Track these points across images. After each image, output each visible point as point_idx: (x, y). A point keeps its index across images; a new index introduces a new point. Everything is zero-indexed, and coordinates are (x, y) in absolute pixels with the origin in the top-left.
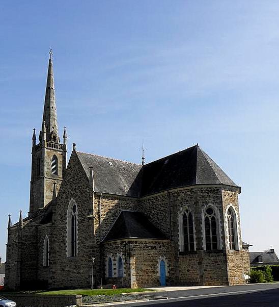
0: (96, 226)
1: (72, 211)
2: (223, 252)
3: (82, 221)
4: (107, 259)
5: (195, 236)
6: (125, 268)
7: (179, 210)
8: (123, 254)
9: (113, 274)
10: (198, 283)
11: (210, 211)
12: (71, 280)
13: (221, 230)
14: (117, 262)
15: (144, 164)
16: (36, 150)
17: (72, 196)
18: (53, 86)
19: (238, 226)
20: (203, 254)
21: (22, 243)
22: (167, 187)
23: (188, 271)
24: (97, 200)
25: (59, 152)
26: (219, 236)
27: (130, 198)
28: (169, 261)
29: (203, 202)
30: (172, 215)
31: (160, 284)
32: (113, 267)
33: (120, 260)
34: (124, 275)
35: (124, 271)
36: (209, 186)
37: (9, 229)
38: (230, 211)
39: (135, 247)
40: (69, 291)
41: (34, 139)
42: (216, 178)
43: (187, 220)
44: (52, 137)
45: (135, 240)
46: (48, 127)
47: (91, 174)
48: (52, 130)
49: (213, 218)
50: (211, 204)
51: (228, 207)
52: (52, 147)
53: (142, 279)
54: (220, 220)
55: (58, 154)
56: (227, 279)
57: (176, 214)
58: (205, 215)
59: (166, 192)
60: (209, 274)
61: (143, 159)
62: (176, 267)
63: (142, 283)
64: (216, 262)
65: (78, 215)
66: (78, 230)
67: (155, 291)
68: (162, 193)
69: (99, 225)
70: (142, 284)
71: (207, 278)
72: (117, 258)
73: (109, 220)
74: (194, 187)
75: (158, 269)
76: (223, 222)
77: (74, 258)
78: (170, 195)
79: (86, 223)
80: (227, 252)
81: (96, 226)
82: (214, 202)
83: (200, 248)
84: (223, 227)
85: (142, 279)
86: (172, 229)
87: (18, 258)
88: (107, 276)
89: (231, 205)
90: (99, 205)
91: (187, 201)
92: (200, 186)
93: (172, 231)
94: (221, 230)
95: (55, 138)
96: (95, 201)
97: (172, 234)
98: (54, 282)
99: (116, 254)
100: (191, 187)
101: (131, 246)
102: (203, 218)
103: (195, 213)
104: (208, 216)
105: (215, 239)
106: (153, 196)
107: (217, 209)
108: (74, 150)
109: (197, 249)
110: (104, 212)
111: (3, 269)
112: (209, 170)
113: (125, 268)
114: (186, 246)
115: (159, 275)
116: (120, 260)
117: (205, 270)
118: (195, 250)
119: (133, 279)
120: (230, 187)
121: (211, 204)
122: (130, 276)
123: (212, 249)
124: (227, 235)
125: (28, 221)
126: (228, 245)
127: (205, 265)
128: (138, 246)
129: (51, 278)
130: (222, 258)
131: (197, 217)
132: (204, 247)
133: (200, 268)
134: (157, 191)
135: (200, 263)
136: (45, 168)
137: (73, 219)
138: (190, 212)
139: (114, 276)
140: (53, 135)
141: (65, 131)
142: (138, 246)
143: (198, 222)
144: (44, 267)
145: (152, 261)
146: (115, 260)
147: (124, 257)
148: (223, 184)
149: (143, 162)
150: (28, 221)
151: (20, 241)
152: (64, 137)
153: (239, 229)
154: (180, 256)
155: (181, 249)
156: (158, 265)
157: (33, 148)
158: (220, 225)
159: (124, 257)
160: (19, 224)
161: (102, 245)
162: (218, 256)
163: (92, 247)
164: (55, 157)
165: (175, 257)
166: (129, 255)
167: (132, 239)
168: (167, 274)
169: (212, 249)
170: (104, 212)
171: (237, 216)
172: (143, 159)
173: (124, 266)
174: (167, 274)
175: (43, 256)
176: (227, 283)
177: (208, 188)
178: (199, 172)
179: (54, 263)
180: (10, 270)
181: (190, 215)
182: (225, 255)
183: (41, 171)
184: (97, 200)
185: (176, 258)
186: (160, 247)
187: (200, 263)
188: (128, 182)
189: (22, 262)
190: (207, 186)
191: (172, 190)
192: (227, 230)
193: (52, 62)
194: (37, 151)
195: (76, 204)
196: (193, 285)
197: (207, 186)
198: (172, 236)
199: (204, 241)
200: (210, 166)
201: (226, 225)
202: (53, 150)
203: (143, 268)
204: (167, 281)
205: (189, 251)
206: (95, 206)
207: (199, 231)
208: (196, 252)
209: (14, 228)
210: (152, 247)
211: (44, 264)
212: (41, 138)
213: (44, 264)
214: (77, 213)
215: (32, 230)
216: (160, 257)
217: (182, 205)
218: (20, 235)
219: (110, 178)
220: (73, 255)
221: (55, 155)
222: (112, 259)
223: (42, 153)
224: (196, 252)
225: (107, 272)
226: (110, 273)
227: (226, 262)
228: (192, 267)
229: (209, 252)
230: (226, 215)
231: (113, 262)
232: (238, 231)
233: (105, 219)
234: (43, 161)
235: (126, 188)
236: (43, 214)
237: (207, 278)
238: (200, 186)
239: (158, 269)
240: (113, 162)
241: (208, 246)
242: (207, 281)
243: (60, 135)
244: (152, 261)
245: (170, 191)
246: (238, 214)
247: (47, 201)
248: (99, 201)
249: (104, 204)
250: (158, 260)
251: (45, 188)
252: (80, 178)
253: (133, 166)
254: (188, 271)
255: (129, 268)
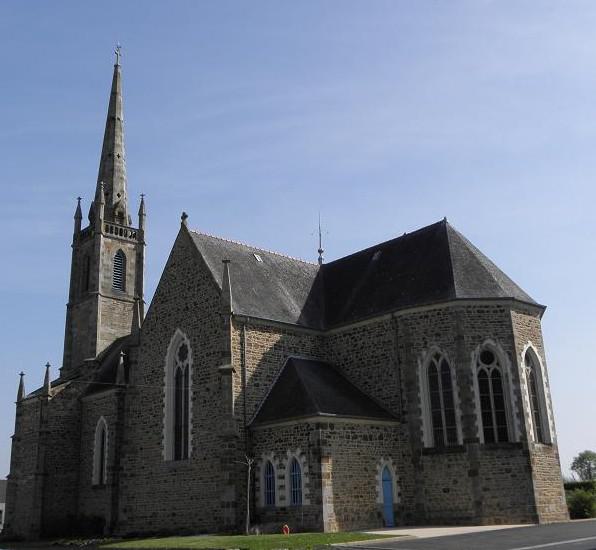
0: (236, 390)
1: (178, 358)
2: (522, 447)
3: (202, 380)
4: (262, 466)
5: (458, 413)
6: (307, 485)
7: (420, 355)
8: (302, 454)
9: (277, 498)
10: (468, 518)
11: (488, 357)
12: (174, 515)
13: (514, 398)
14: (286, 472)
15: (324, 263)
16: (81, 240)
17: (178, 324)
18: (121, 115)
19: (546, 389)
20: (479, 452)
21: (48, 433)
22: (390, 303)
23: (446, 491)
24: (238, 332)
25: (129, 245)
26: (512, 410)
27: (307, 331)
28: (401, 470)
29: (473, 338)
30: (403, 366)
31: (384, 522)
32: (278, 482)
33: (295, 463)
34: (306, 502)
35: (305, 491)
36: (485, 303)
37: (20, 403)
38: (530, 358)
39: (330, 437)
40: (205, 537)
41: (78, 217)
42: (496, 287)
43: (440, 378)
44: (116, 214)
45: (329, 420)
46: (109, 194)
47: (225, 277)
48: (116, 199)
49: (496, 373)
50: (489, 341)
51: (526, 348)
52: (112, 232)
53: (346, 510)
54: (511, 377)
55: (128, 248)
56: (534, 509)
57: (412, 364)
58: (478, 365)
59: (388, 317)
60: (493, 497)
61: (320, 252)
62: (416, 482)
63: (346, 519)
64: (508, 471)
65: (193, 366)
66: (194, 399)
67: (378, 540)
68: (378, 320)
69: (243, 388)
70: (348, 522)
71: (490, 506)
72: (287, 463)
73: (264, 376)
74: (450, 304)
75: (379, 488)
76: (517, 380)
77: (182, 463)
78: (396, 322)
79: (212, 384)
80: (530, 448)
81: (236, 390)
82: (497, 336)
83: (471, 439)
84: (518, 393)
85: (346, 510)
86: (404, 398)
87: (38, 467)
88: (262, 503)
89: (530, 344)
90: (242, 343)
91: (438, 335)
92: (466, 303)
93: (403, 402)
94: (514, 398)
95: (121, 216)
96: (234, 334)
97: (405, 409)
98: (131, 519)
99: (284, 452)
100: (444, 306)
101: (323, 433)
102: (475, 371)
103: (456, 361)
104: (485, 367)
105: (502, 418)
106: (355, 325)
107: (501, 350)
108: (183, 226)
109: (464, 441)
110: (254, 359)
111: (2, 491)
112: (479, 269)
113: (307, 485)
114: (437, 434)
115: (380, 500)
116: (295, 463)
117: (485, 489)
118: (461, 443)
119: (328, 509)
120: (526, 307)
121: (489, 341)
122: (320, 502)
123: (496, 439)
124: (528, 409)
125: (62, 387)
126: (532, 433)
127: (484, 477)
128: (335, 433)
129: (125, 511)
130: (516, 462)
131: (461, 371)
132: (480, 435)
133: (475, 485)
134: (365, 315)
135: (473, 473)
136: (101, 276)
137: (180, 377)
138: (444, 360)
139: (279, 504)
140: (118, 209)
141: (142, 202)
142: (335, 433)
143: (466, 380)
144: (95, 488)
145: (366, 469)
146: (281, 466)
147: (304, 459)
148: (513, 299)
149: (320, 259)
150: (62, 387)
151: (43, 429)
152: (141, 214)
153: (549, 396)
154: (425, 457)
155: (427, 440)
156: (379, 478)
157: (75, 235)
158: (512, 387)
159: (304, 459)
160: (42, 393)
161: (249, 431)
162: (512, 456)
163: (227, 438)
164: (121, 255)
165: (413, 459)
166: (318, 456)
167: (326, 417)
168: (397, 500)
169: (496, 439)
170: (254, 359)
171: (543, 368)
172: (320, 252)
173: (305, 480)
174: (397, 500)
175: (92, 461)
176: (535, 519)
177: (481, 307)
178: (458, 274)
179: (132, 475)
180: (18, 493)
181: (445, 366)
182: (527, 454)
183: (91, 281)
184: (238, 332)
185: (415, 461)
186: (381, 438)
187: (473, 473)
188: (297, 298)
189: (46, 475)
190: (479, 303)
191: (401, 313)
192: (527, 398)
193: (119, 70)
194: (84, 245)
195: (188, 342)
196: (458, 524)
197: (479, 303)
198: (404, 413)
199: (479, 423)
200: (479, 263)
201: (525, 387)
202: (117, 239)
203: (348, 485)
204: (396, 514)
205: (445, 447)
206: (234, 344)
207: (467, 402)
208: (462, 449)
209: (27, 402)
210: (365, 438)
211: (95, 480)
212: (93, 215)
213: (95, 480)
214: (190, 361)
215: (69, 405)
216: (382, 460)
217: (426, 343)
218: (45, 415)
219: (262, 288)
220: (177, 456)
221: (120, 250)
222: (275, 464)
223: (96, 245)
224: (462, 449)
225: (262, 495)
226: (270, 498)
227: (529, 469)
228: (455, 482)
229: (491, 449)
230: (522, 365)
231: (277, 472)
232: (547, 402)
233: (255, 376)
234: (96, 261)
235: (296, 310)
236: (93, 371)
237: (490, 506)
238: (466, 303)
239: (379, 488)
240: (262, 255)
241: (488, 434)
242: (492, 514)
243: (131, 213)
244: (366, 469)
245: (397, 314)
246: (544, 363)
247: (102, 345)
248: (242, 336)
249: (253, 341)
250: (378, 467)
251: (99, 316)
252: (198, 285)
253: (301, 265)
254: (446, 491)
255: (319, 485)
